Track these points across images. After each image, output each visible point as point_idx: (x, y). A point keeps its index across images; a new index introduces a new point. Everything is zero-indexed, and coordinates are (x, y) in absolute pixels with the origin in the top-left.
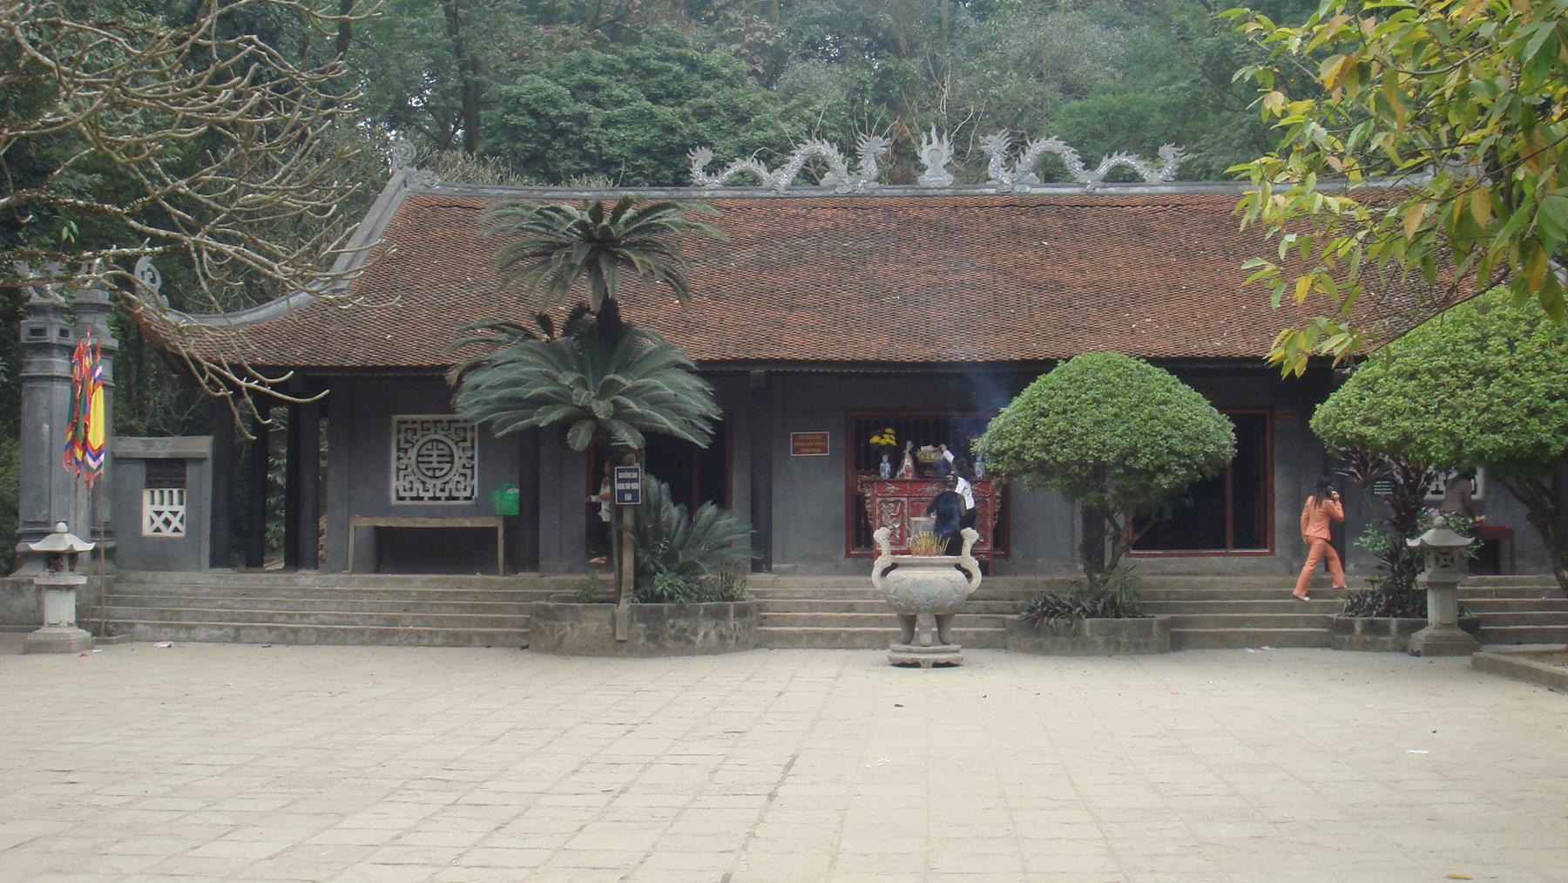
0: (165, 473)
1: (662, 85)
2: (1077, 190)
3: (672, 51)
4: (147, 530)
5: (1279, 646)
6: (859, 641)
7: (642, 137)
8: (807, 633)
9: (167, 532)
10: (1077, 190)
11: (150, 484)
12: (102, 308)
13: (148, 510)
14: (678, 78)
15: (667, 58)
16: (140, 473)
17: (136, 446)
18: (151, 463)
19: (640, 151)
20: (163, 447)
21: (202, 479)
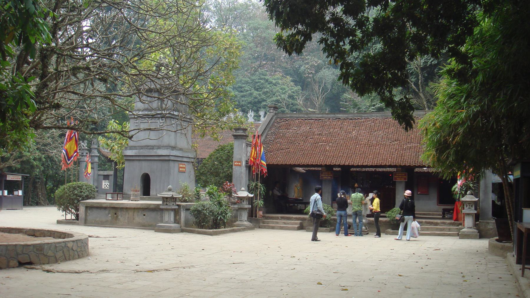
0: (106, 177)
1: (258, 86)
2: (495, 124)
3: (263, 77)
4: (103, 187)
5: (189, 232)
6: (122, 217)
7: (250, 99)
8: (170, 223)
9: (106, 188)
10: (495, 124)
11: (104, 179)
12: (97, 156)
13: (103, 184)
14: (262, 84)
15: (261, 79)
16: (102, 177)
17: (102, 173)
18: (104, 175)
19: (250, 103)
20: (106, 173)
21: (112, 178)
